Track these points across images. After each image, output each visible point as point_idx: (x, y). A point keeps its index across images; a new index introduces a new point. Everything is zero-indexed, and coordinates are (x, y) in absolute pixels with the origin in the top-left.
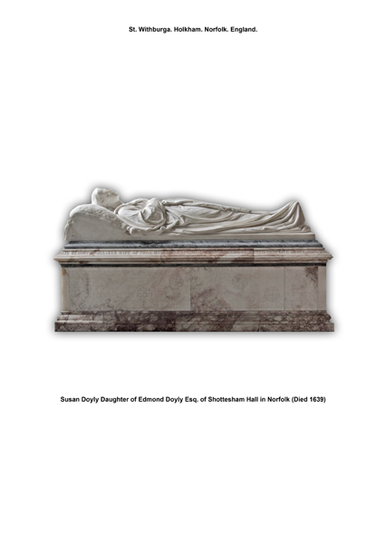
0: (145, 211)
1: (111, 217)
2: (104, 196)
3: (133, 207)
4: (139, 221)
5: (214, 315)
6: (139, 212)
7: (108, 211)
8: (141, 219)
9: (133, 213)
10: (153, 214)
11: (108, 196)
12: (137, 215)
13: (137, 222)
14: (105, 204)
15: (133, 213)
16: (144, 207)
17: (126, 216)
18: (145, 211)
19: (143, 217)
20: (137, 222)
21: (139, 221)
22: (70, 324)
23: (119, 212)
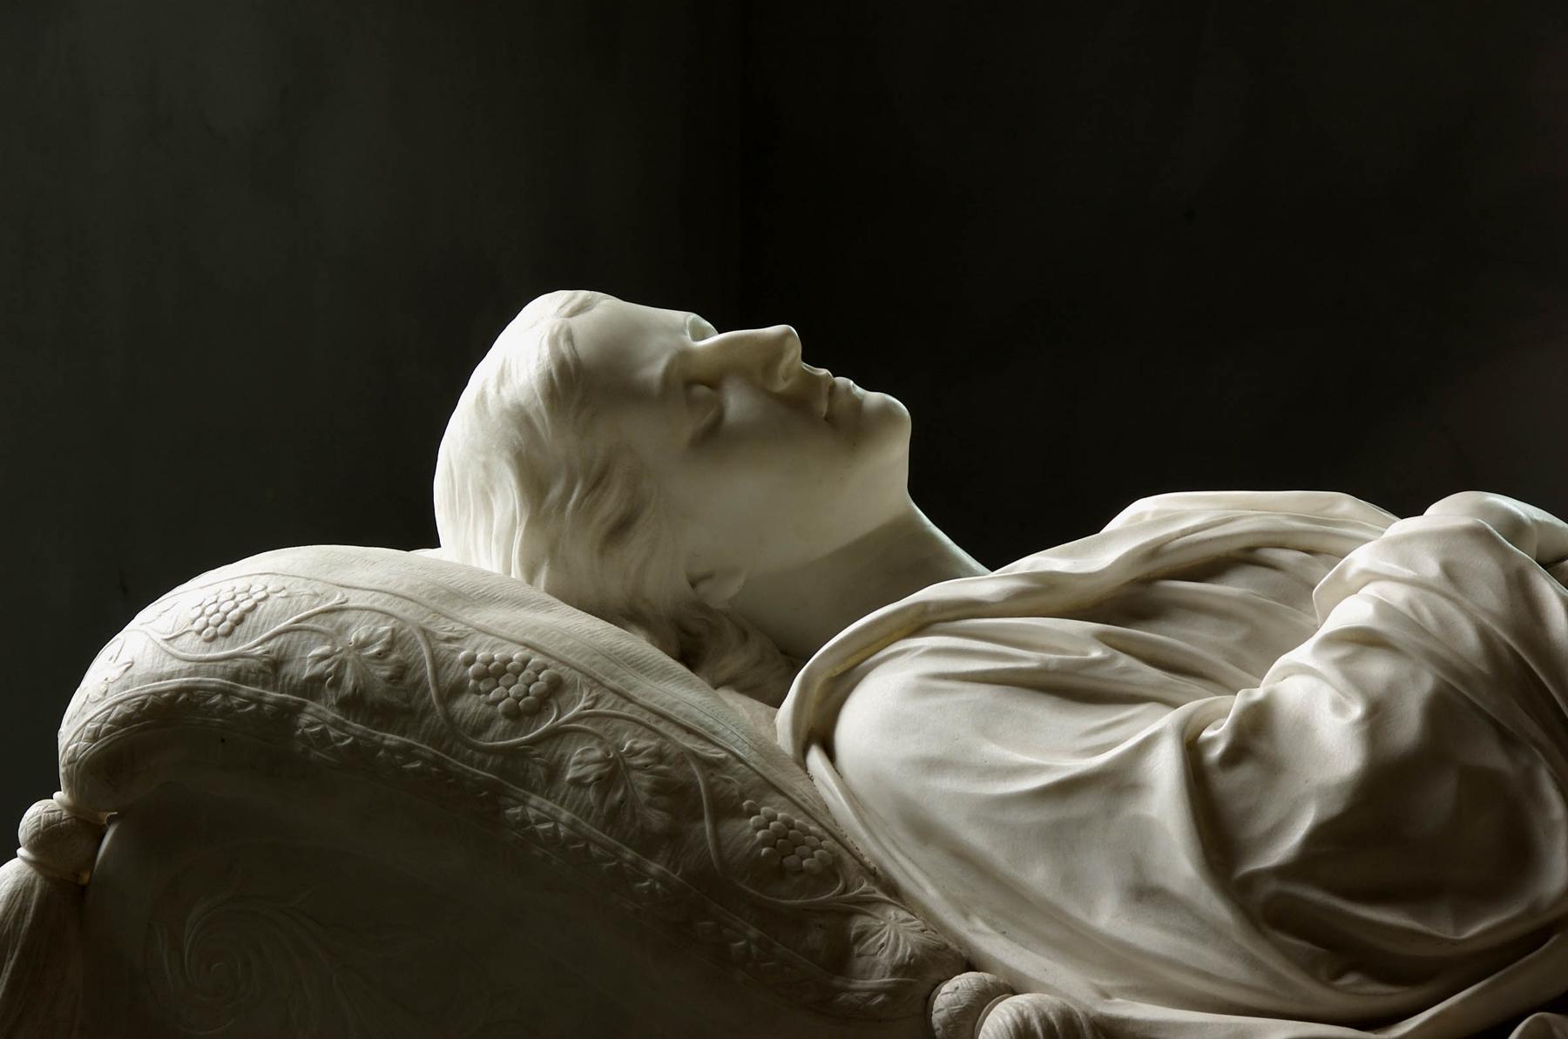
0: (1256, 728)
1: (691, 791)
2: (653, 438)
3: (1075, 641)
4: (1146, 894)
5: (830, 407)
6: (1151, 737)
7: (683, 694)
8: (1177, 859)
9: (1064, 744)
10: (1386, 784)
11: (713, 437)
12: (1118, 782)
13: (1109, 916)
14: (656, 567)
15: (1064, 744)
16: (1264, 646)
17: (947, 797)
18: (1256, 728)
19: (1217, 828)
20: (1109, 916)
21: (1146, 894)
22: (936, 886)
23: (865, 719)
